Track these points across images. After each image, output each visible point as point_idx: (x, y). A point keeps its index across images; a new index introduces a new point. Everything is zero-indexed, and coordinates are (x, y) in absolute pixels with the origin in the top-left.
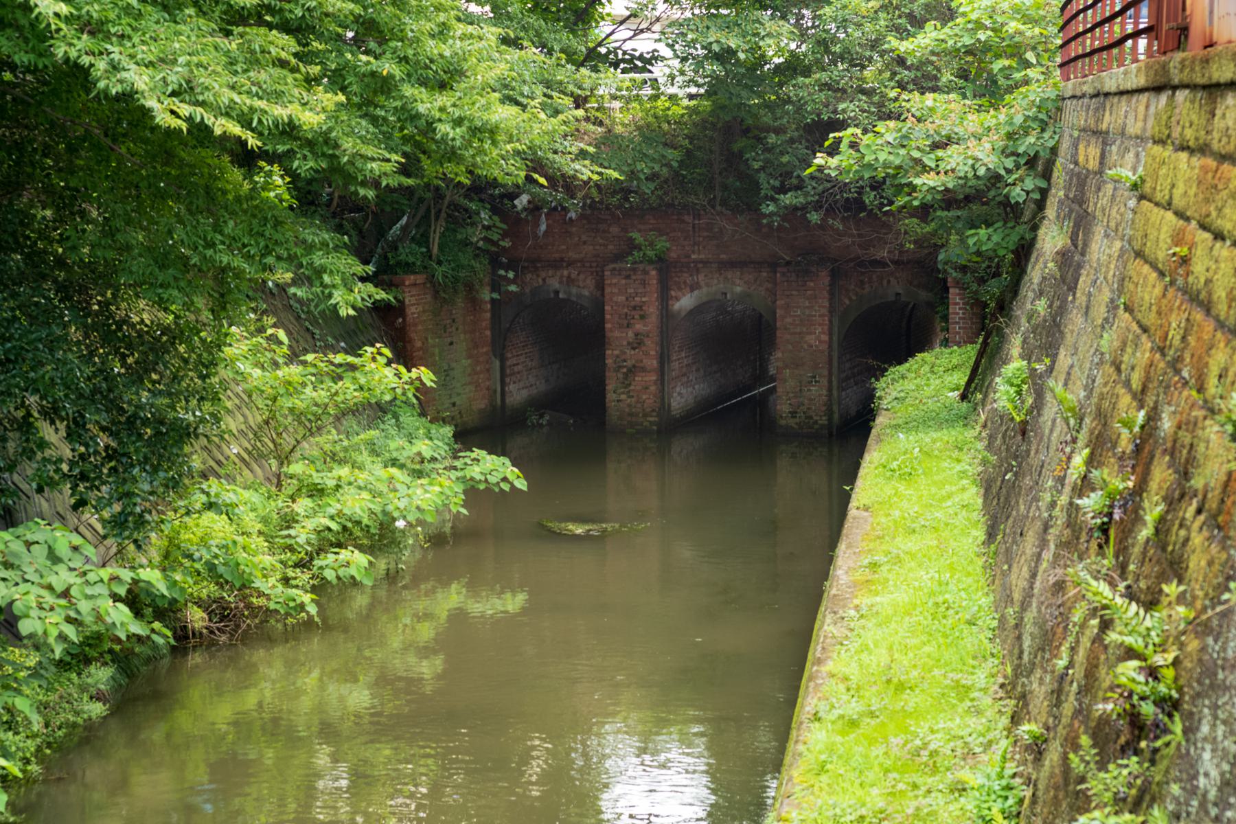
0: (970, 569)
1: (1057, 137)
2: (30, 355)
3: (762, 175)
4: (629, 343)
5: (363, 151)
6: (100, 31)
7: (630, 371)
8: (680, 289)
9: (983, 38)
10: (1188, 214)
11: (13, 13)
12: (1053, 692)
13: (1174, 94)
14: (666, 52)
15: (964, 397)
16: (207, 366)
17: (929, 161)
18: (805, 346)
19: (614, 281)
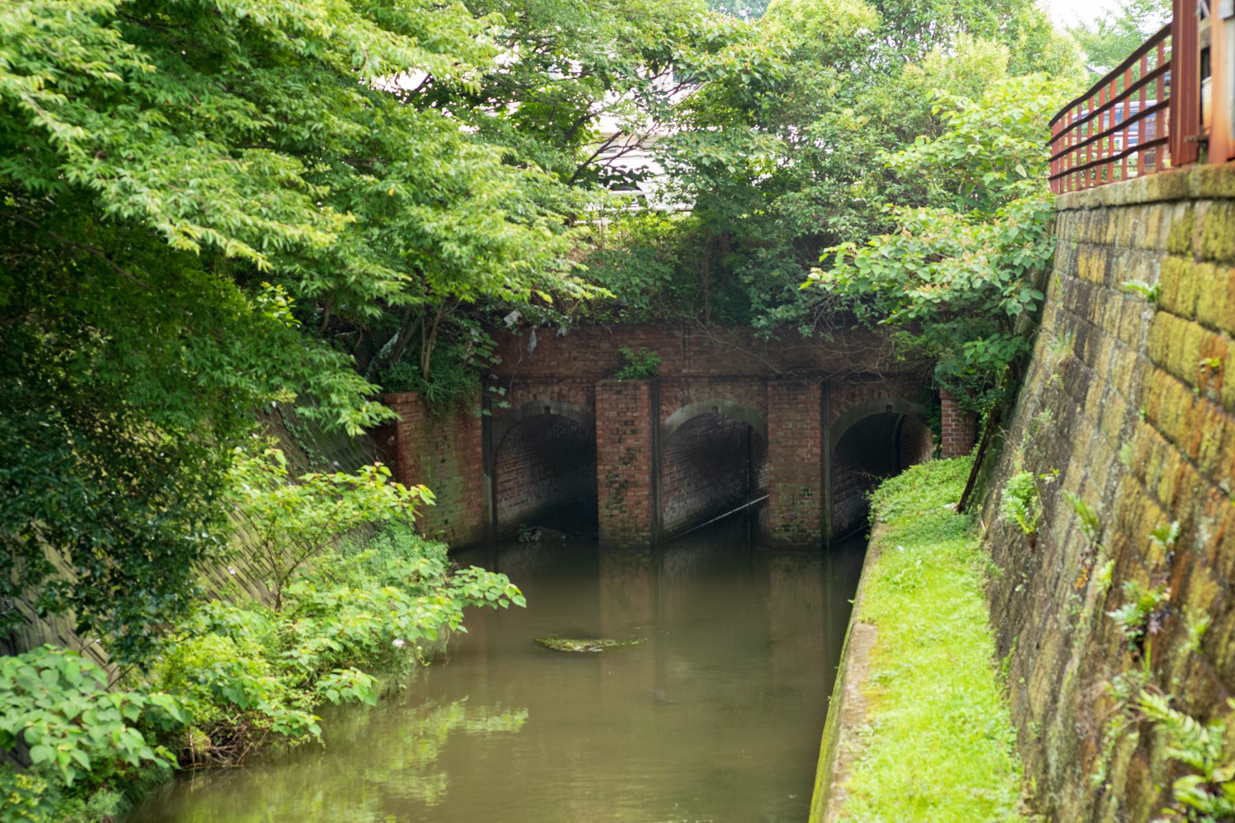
0: (983, 682)
1: (1052, 249)
2: (37, 479)
4: (621, 459)
5: (370, 271)
6: (111, 155)
7: (622, 486)
8: (671, 404)
9: (973, 152)
10: (1218, 324)
11: (24, 138)
12: (1088, 807)
13: (1193, 206)
14: (656, 168)
15: (961, 509)
16: (214, 486)
17: (924, 274)
19: (605, 396)
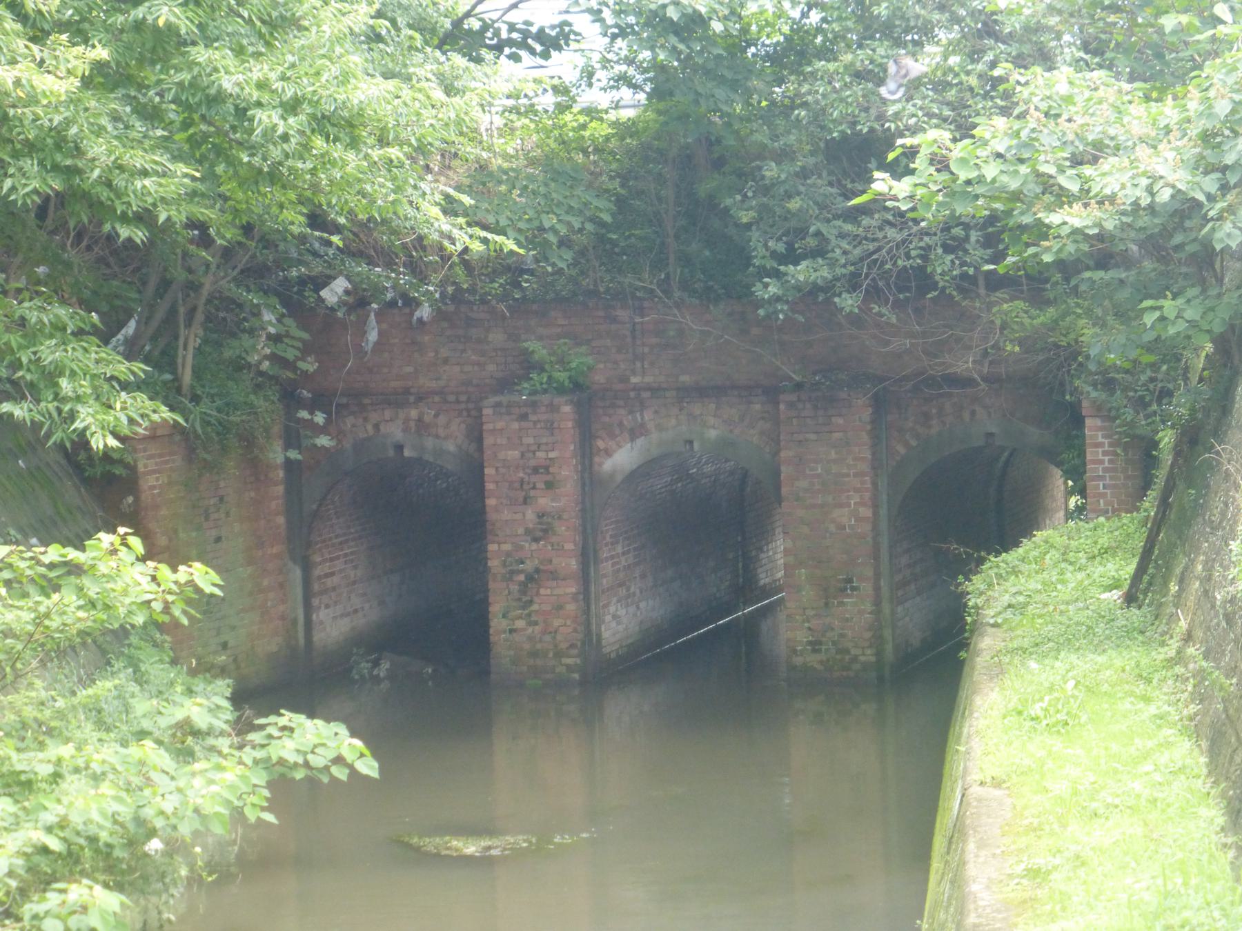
3: (755, 234)
4: (528, 531)
7: (530, 578)
8: (612, 436)
15: (1130, 599)
18: (832, 528)
19: (500, 425)
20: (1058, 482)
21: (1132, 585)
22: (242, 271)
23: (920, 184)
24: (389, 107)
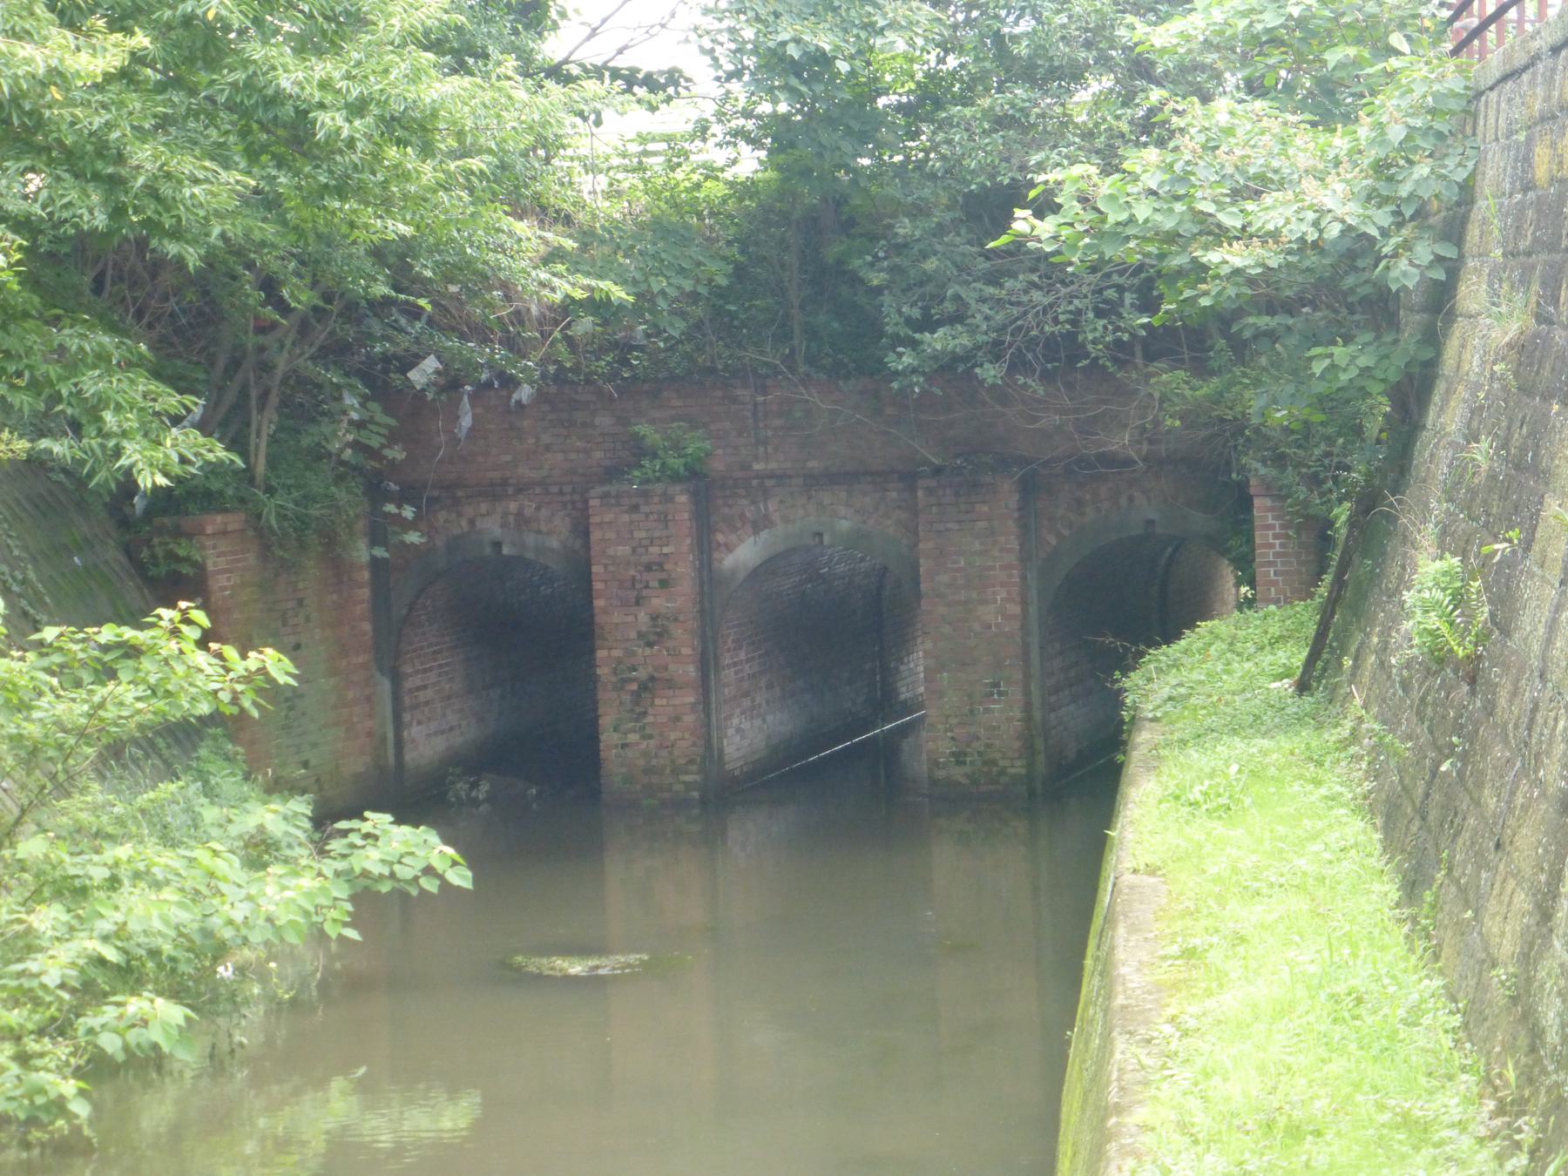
1: (1470, 165)
4: (640, 635)
7: (644, 687)
8: (734, 529)
15: (1303, 687)
17: (1230, 220)
19: (609, 517)
20: (1227, 574)
21: (1304, 673)
22: (320, 349)
23: (1065, 224)
24: (466, 109)
